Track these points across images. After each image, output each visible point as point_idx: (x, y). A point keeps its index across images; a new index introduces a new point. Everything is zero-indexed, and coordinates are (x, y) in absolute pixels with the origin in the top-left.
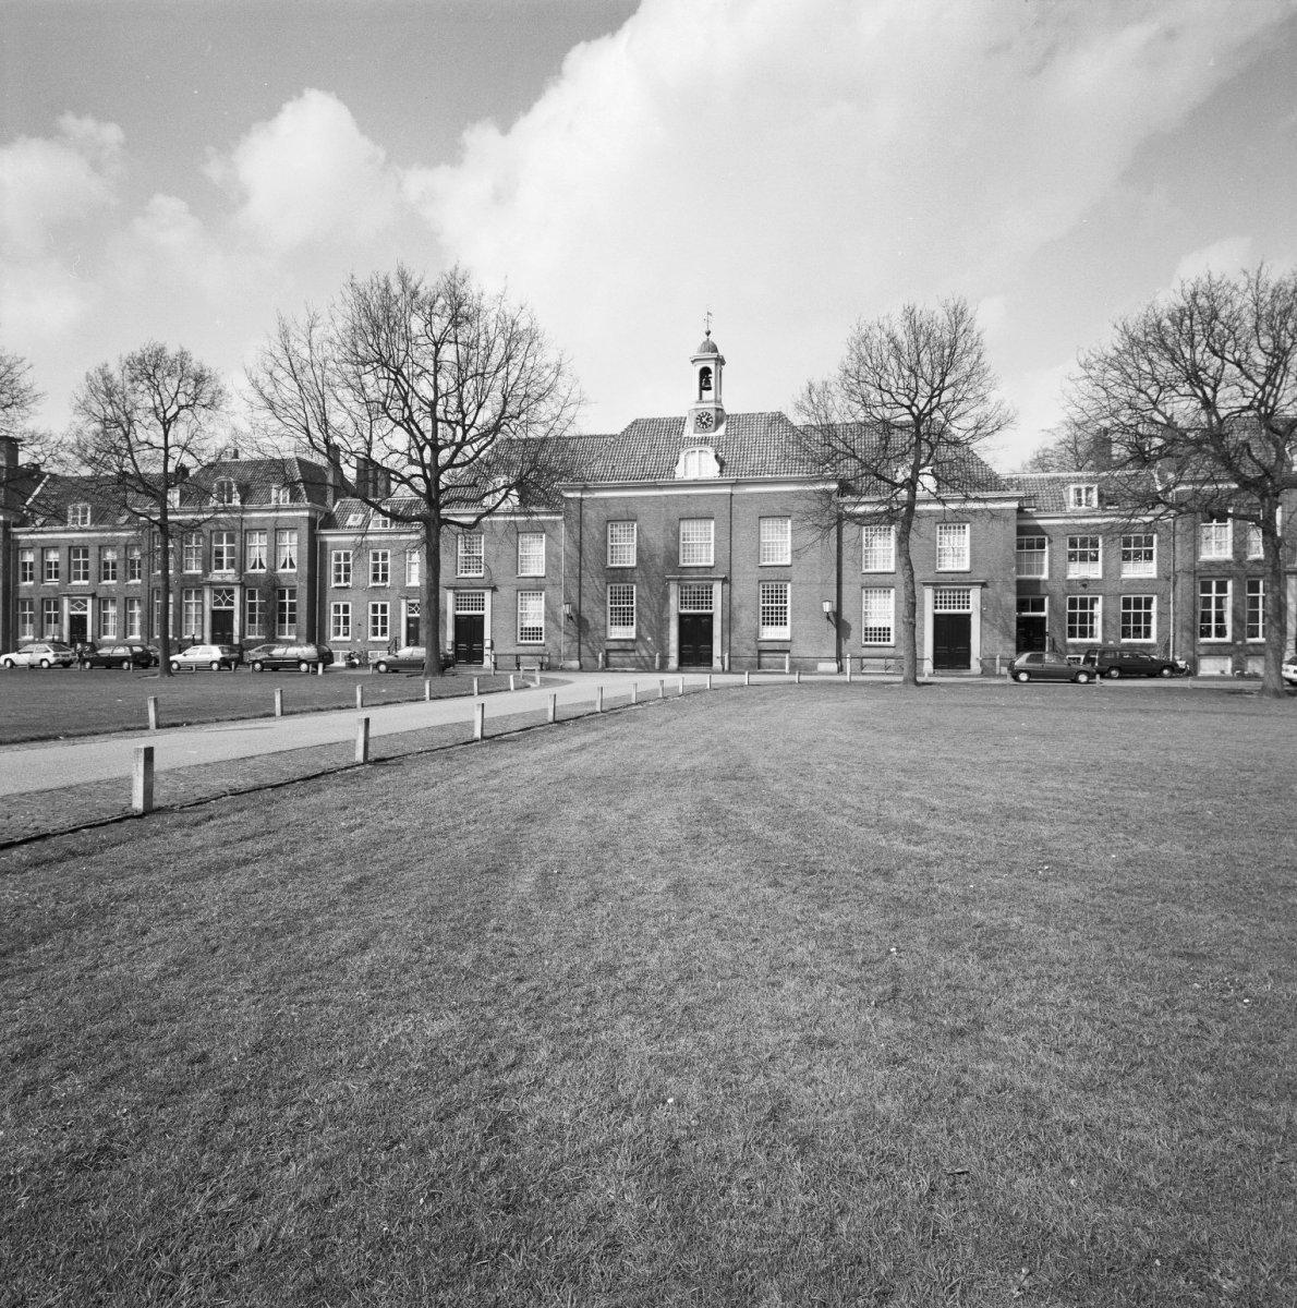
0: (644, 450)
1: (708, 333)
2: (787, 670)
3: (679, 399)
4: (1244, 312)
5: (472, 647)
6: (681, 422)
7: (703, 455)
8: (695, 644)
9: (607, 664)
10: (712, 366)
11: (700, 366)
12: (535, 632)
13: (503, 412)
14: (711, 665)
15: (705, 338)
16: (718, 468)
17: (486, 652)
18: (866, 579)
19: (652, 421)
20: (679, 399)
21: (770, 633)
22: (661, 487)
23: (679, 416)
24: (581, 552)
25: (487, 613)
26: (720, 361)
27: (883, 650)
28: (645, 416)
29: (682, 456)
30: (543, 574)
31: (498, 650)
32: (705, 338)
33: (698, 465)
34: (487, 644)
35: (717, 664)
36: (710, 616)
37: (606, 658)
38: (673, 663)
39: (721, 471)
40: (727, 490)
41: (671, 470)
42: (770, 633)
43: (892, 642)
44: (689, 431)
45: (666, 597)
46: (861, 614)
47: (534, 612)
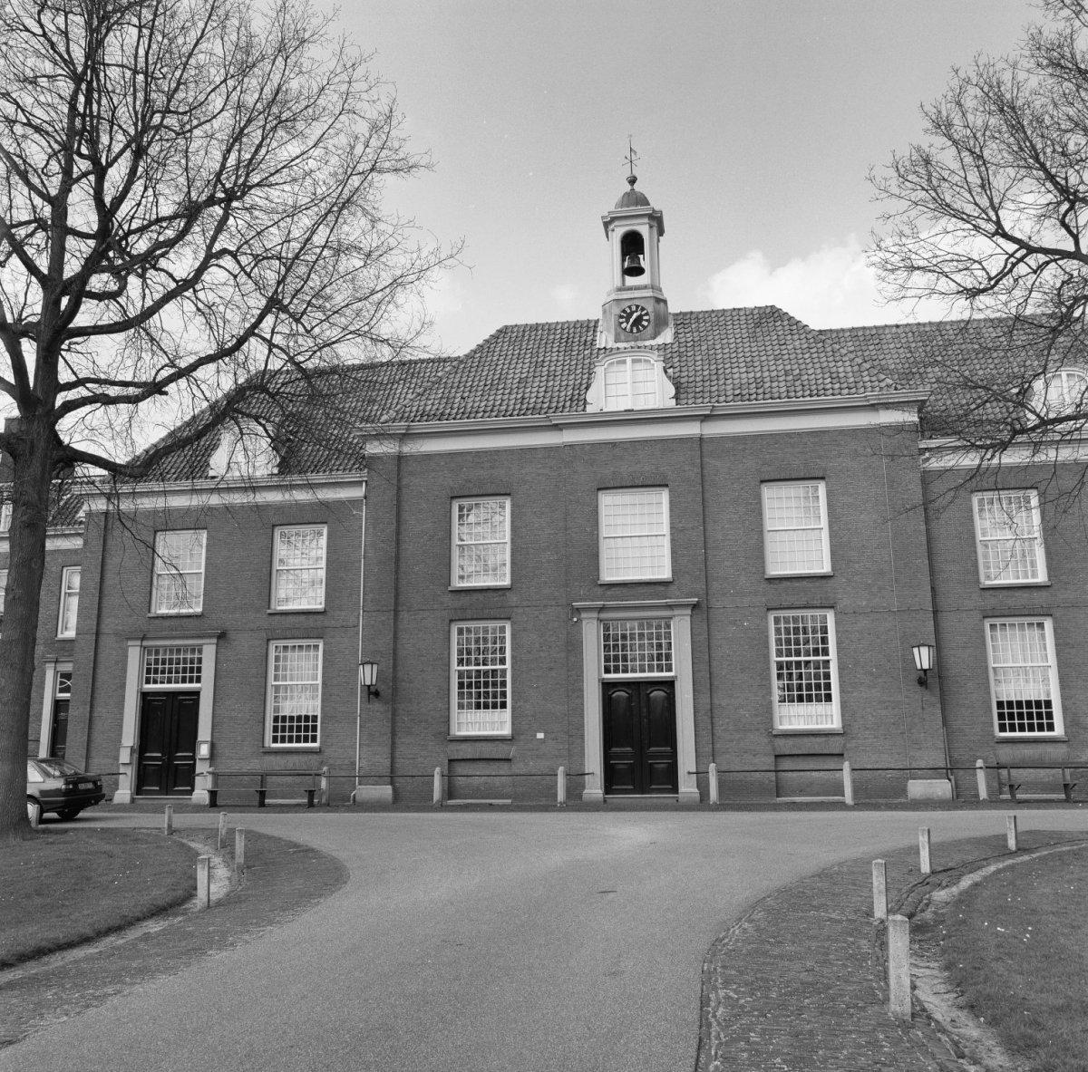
0: (523, 369)
1: (633, 181)
2: (848, 798)
3: (581, 288)
4: (925, 995)
5: (172, 758)
6: (591, 327)
7: (638, 366)
8: (639, 747)
9: (450, 792)
10: (644, 230)
11: (619, 231)
12: (302, 726)
13: (275, 98)
14: (675, 789)
15: (628, 188)
16: (672, 391)
17: (201, 767)
18: (991, 601)
19: (536, 327)
20: (581, 288)
21: (795, 717)
22: (558, 427)
23: (583, 317)
24: (397, 589)
25: (206, 687)
26: (657, 220)
27: (1041, 748)
28: (521, 321)
29: (600, 371)
30: (321, 607)
31: (229, 765)
32: (628, 188)
33: (632, 385)
34: (204, 750)
35: (687, 787)
36: (669, 685)
37: (449, 777)
38: (594, 788)
39: (677, 397)
40: (692, 429)
41: (579, 400)
42: (795, 717)
43: (1059, 731)
44: (604, 339)
45: (573, 647)
46: (981, 673)
47: (299, 683)
